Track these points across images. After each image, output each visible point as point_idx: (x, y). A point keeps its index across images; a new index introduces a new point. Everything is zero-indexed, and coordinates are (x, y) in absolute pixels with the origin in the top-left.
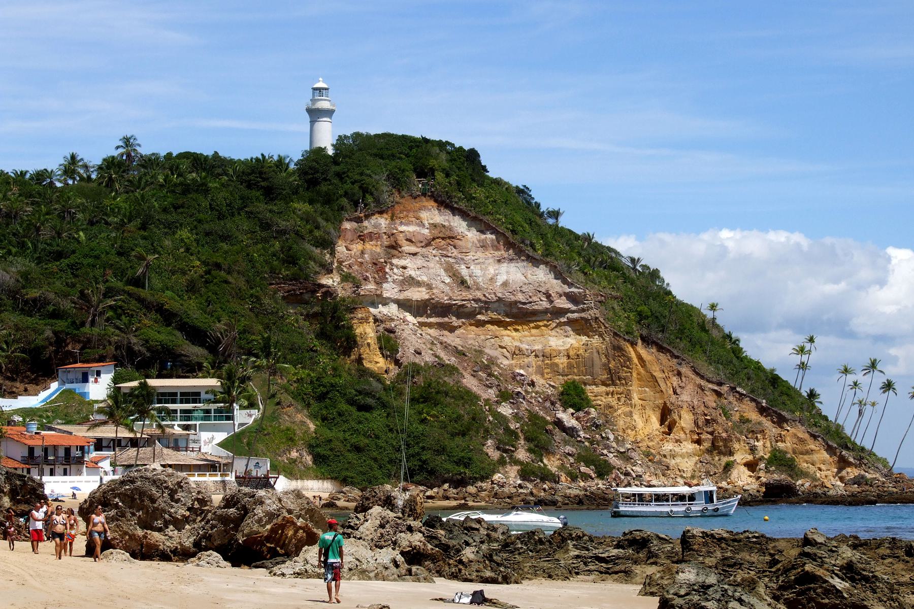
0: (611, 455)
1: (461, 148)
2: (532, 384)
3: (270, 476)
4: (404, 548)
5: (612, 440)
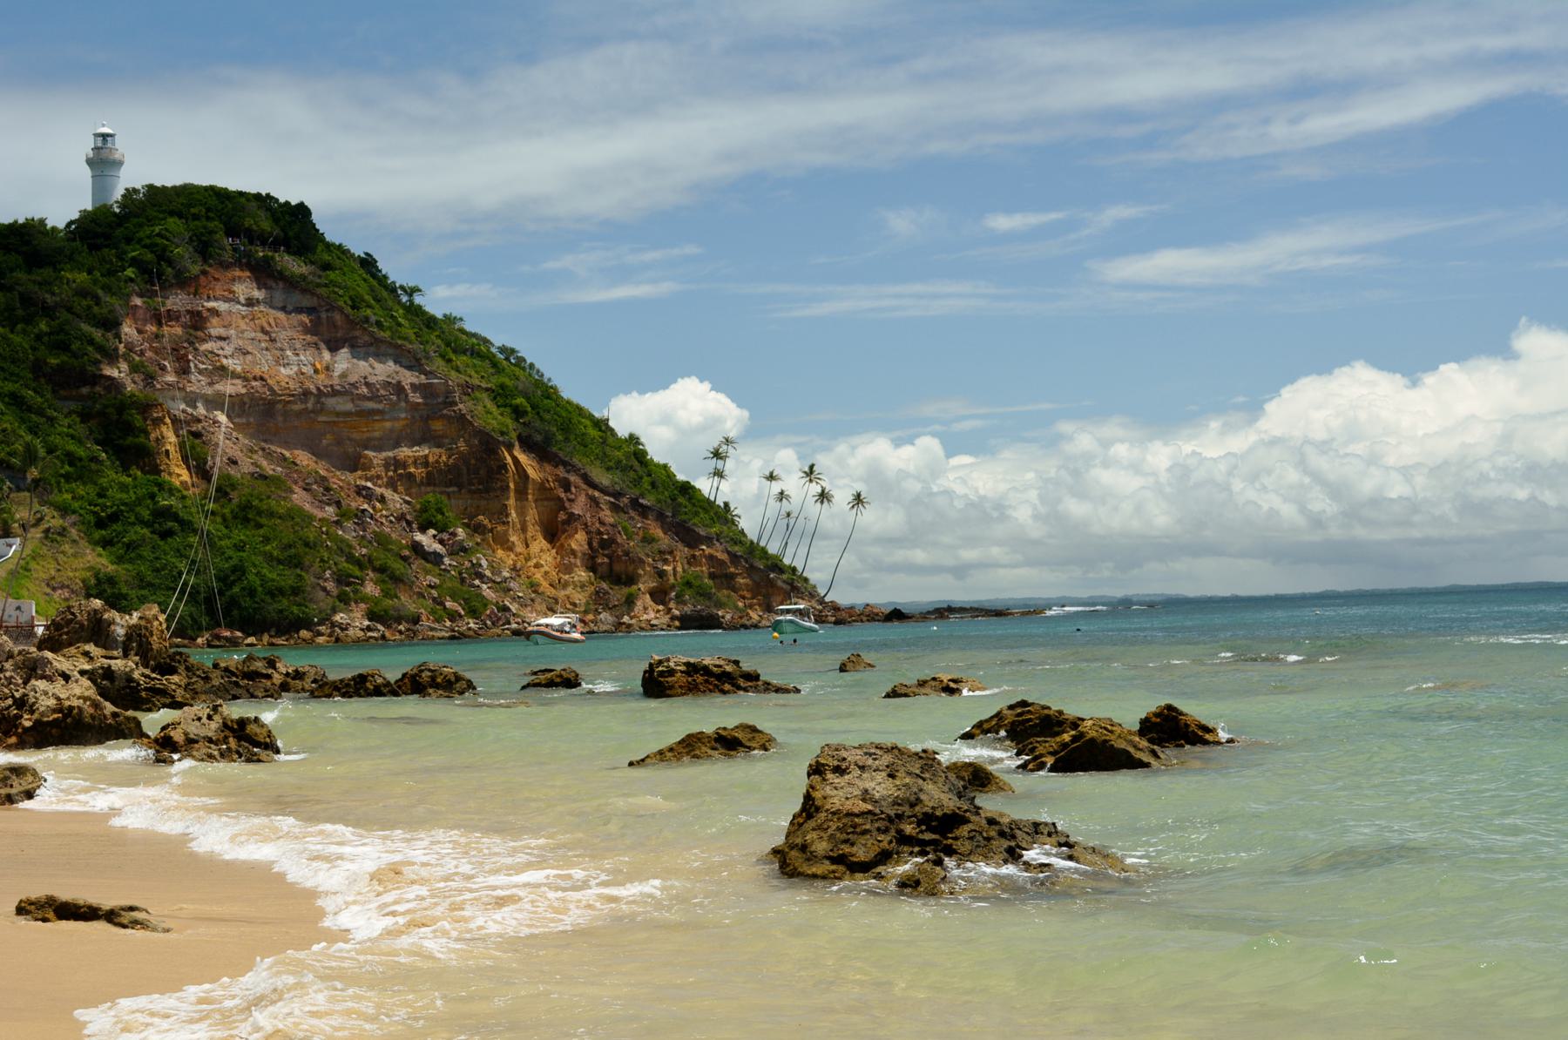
0: (485, 586)
1: (287, 203)
2: (382, 499)
3: (36, 623)
4: (42, 714)
5: (485, 567)
